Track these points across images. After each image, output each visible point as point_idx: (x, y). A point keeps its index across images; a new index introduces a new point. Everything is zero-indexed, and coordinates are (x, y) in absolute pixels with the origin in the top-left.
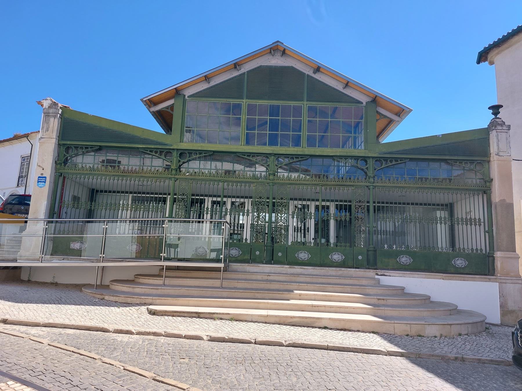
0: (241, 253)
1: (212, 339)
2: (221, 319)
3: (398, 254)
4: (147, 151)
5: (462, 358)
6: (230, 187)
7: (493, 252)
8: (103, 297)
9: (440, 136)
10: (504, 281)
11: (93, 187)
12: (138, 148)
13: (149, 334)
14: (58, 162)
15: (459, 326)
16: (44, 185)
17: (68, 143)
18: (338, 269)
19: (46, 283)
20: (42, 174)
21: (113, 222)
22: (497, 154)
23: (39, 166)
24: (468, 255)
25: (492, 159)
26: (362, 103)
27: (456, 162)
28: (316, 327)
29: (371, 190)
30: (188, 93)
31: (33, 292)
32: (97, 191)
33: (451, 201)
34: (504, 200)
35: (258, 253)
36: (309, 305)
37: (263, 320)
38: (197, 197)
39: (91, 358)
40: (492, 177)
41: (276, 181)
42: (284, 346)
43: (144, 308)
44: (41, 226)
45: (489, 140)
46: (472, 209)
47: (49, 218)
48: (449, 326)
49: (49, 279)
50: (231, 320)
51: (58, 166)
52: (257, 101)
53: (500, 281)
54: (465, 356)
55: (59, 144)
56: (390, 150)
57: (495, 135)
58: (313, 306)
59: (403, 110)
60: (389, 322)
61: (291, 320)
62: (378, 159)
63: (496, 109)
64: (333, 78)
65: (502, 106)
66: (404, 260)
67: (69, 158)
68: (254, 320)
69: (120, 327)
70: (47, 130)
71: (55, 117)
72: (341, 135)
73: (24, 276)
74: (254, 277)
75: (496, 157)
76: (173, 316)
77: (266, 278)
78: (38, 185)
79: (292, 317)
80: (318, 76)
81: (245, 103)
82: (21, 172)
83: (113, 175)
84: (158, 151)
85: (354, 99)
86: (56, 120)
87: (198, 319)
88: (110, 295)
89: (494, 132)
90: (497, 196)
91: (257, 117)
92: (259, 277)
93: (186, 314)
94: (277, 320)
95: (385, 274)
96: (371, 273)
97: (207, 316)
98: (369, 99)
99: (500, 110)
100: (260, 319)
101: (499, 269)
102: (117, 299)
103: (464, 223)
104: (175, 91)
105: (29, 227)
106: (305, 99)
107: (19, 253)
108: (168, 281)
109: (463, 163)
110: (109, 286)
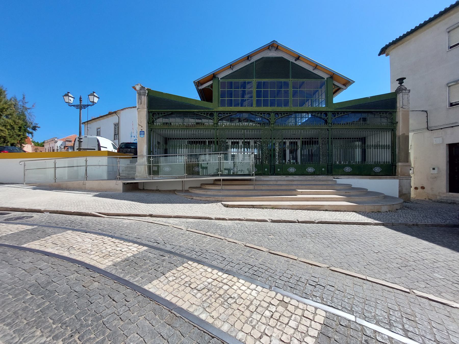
0: (257, 170)
1: (273, 221)
2: (267, 208)
3: (345, 166)
4: (199, 113)
5: (417, 224)
6: (248, 132)
7: (395, 163)
8: (192, 197)
9: (369, 98)
10: (402, 178)
11: (166, 137)
12: (194, 112)
13: (236, 220)
14: (149, 122)
15: (396, 205)
16: (144, 136)
17: (154, 110)
18: (313, 176)
19: (154, 190)
20: (142, 130)
21: (174, 156)
22: (402, 107)
23: (139, 125)
24: (382, 165)
25: (398, 110)
26: (324, 79)
27: (377, 113)
28: (321, 210)
29: (330, 131)
30: (220, 76)
31: (156, 196)
32: (168, 139)
33: (364, 136)
34: (404, 134)
35: (266, 170)
36: (311, 198)
37: (290, 207)
38: (197, 140)
39: (219, 238)
40: (397, 121)
41: (275, 128)
42: (315, 223)
43: (219, 204)
44: (145, 160)
45: (396, 99)
46: (381, 140)
47: (149, 155)
48: (392, 206)
49: (155, 188)
50: (272, 208)
51: (150, 125)
52: (262, 80)
53: (400, 178)
54: (418, 223)
55: (149, 112)
56: (341, 107)
57: (401, 96)
58: (313, 198)
59: (350, 82)
60: (362, 205)
61: (307, 207)
62: (334, 112)
63: (401, 80)
64: (307, 63)
65: (405, 78)
66: (348, 169)
67: (154, 120)
68: (285, 208)
69: (218, 217)
70: (141, 103)
71: (144, 95)
72: (269, 98)
73: (140, 187)
74: (268, 183)
75: (401, 109)
76: (239, 208)
77: (275, 183)
78: (140, 136)
79: (307, 206)
80: (298, 63)
81: (254, 81)
82: (115, 130)
83: (181, 129)
84: (205, 113)
85: (319, 76)
86: (146, 97)
87: (253, 209)
88: (197, 197)
89: (401, 94)
90: (400, 131)
91: (262, 90)
92: (271, 183)
93: (246, 206)
94: (298, 207)
95: (339, 178)
96: (330, 178)
97: (258, 207)
98: (328, 76)
99: (404, 81)
100: (288, 207)
101: (399, 172)
102: (201, 198)
103: (381, 148)
104: (213, 75)
105: (139, 160)
106: (291, 77)
107: (136, 175)
108: (224, 187)
109: (381, 113)
110: (188, 190)
